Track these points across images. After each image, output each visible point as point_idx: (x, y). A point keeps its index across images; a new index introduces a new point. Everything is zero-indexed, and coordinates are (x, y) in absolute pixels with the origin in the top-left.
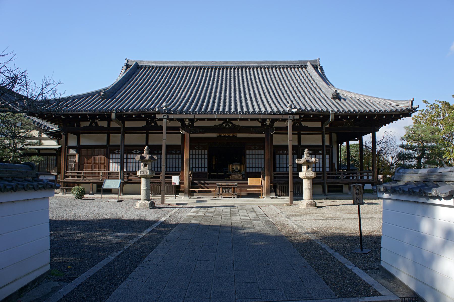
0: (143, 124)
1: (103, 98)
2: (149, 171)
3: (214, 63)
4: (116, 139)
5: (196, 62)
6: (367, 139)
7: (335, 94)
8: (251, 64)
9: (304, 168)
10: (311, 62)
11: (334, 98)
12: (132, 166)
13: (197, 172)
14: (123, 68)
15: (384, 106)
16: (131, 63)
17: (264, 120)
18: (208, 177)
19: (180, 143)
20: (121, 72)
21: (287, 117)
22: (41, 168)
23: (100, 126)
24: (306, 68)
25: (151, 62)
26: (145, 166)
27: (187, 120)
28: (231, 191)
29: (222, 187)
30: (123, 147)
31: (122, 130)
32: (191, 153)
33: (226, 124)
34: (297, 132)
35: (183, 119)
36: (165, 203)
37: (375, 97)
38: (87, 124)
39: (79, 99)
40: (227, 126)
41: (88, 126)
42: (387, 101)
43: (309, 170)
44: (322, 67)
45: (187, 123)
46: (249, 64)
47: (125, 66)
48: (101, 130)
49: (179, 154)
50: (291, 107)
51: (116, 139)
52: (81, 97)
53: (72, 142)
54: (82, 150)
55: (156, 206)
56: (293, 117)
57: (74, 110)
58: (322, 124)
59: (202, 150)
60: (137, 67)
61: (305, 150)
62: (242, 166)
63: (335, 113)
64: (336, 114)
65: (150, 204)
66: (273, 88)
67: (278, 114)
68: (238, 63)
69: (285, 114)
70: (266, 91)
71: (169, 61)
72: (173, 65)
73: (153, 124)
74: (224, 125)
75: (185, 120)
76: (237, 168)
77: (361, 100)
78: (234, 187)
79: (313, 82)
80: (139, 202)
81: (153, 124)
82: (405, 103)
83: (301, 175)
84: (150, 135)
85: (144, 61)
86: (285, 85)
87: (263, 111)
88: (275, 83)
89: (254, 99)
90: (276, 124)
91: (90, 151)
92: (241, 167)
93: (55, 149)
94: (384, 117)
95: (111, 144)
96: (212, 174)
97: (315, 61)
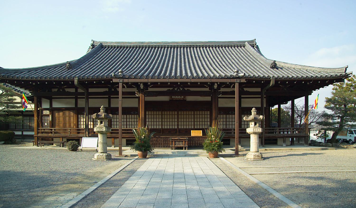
1: (69, 68)
2: (105, 127)
3: (166, 44)
5: (151, 43)
6: (300, 102)
7: (274, 64)
8: (197, 43)
9: (252, 124)
10: (249, 42)
11: (272, 68)
14: (90, 47)
15: (318, 73)
16: (96, 44)
17: (213, 84)
18: (162, 133)
19: (137, 106)
20: (88, 50)
21: (235, 80)
22: (25, 126)
23: (66, 91)
24: (244, 47)
25: (114, 43)
26: (101, 123)
27: (142, 85)
28: (182, 144)
29: (175, 141)
34: (74, 96)
35: (137, 83)
37: (309, 67)
38: (56, 90)
39: (49, 69)
40: (179, 90)
41: (56, 91)
42: (322, 69)
43: (256, 126)
44: (257, 46)
45: (142, 87)
46: (196, 44)
47: (91, 45)
49: (137, 114)
50: (237, 72)
52: (50, 68)
53: (45, 105)
54: (55, 111)
55: (112, 157)
56: (240, 81)
57: (41, 77)
60: (102, 46)
61: (253, 109)
63: (276, 79)
64: (276, 79)
65: (106, 156)
66: (218, 60)
67: (226, 78)
68: (187, 43)
69: (232, 78)
70: (212, 62)
71: (129, 42)
72: (132, 45)
74: (176, 89)
75: (139, 84)
77: (296, 69)
78: (185, 140)
79: (251, 56)
80: (97, 154)
82: (338, 70)
83: (249, 130)
85: (107, 42)
86: (228, 59)
87: (212, 76)
88: (220, 57)
89: (202, 68)
90: (222, 90)
95: (79, 106)
97: (252, 41)
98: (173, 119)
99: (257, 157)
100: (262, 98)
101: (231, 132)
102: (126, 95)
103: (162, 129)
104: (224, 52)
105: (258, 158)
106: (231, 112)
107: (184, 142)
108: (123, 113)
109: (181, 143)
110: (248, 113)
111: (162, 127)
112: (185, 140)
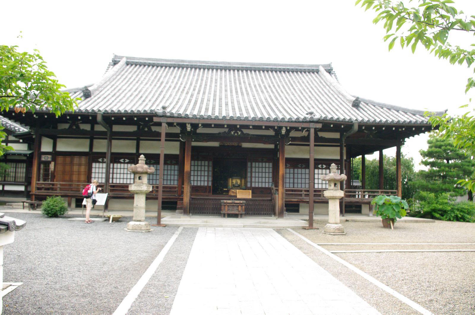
0: (132, 129)
4: (100, 146)
6: (390, 153)
10: (324, 66)
12: (166, 179)
13: (196, 186)
29: (228, 205)
30: (109, 155)
31: (108, 135)
32: (193, 164)
33: (234, 131)
34: (136, 138)
36: (161, 223)
38: (66, 126)
40: (236, 134)
45: (189, 128)
48: (82, 135)
51: (100, 146)
54: (60, 156)
58: (341, 136)
59: (266, 162)
62: (243, 180)
73: (146, 129)
76: (237, 183)
78: (241, 205)
81: (146, 129)
84: (141, 142)
90: (293, 134)
91: (68, 159)
92: (241, 181)
93: (25, 155)
94: (414, 129)
96: (226, 189)
97: (329, 65)
98: (203, 172)
99: (337, 231)
100: (341, 147)
101: (301, 194)
102: (150, 137)
103: (208, 187)
104: (320, 87)
105: (339, 231)
106: (300, 165)
107: (240, 207)
108: (165, 163)
109: (236, 208)
110: (151, 163)
111: (208, 183)
112: (241, 205)
